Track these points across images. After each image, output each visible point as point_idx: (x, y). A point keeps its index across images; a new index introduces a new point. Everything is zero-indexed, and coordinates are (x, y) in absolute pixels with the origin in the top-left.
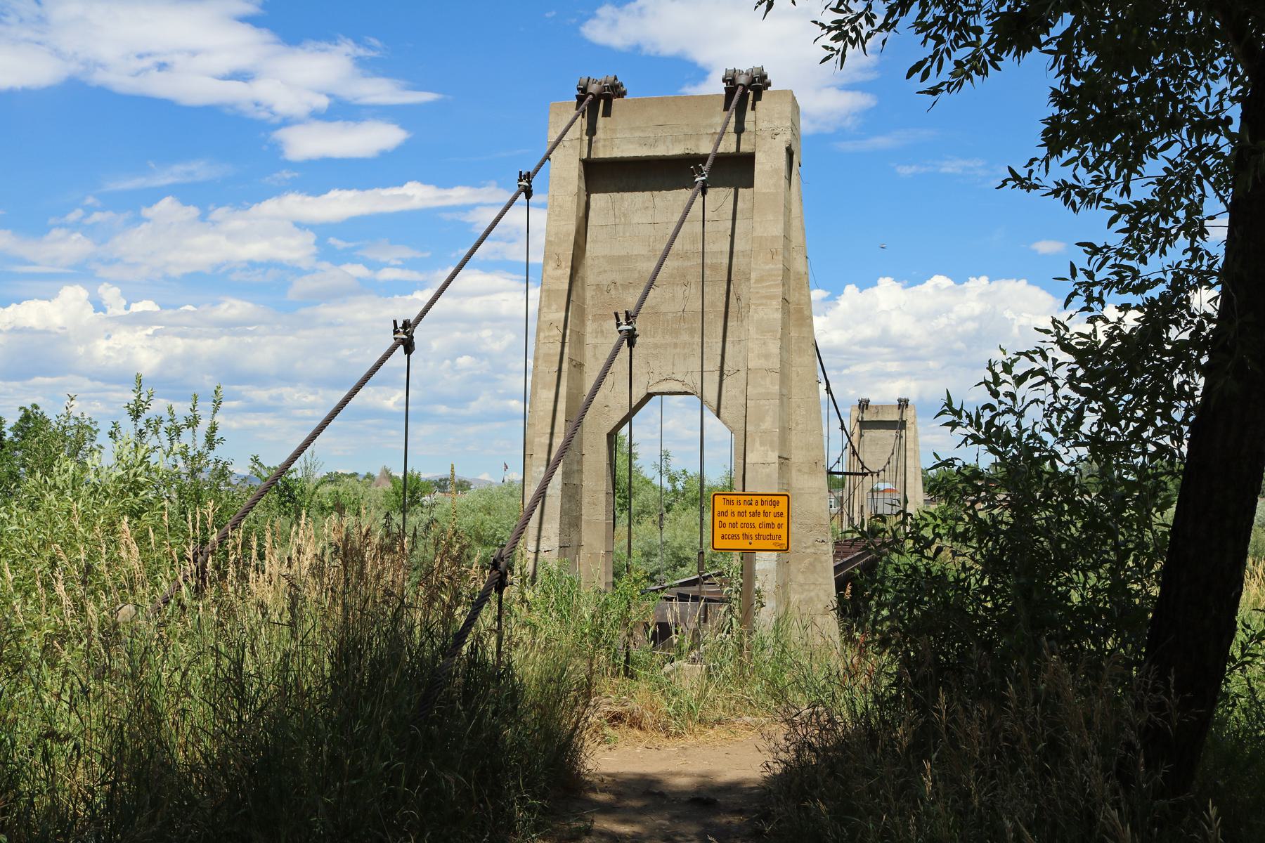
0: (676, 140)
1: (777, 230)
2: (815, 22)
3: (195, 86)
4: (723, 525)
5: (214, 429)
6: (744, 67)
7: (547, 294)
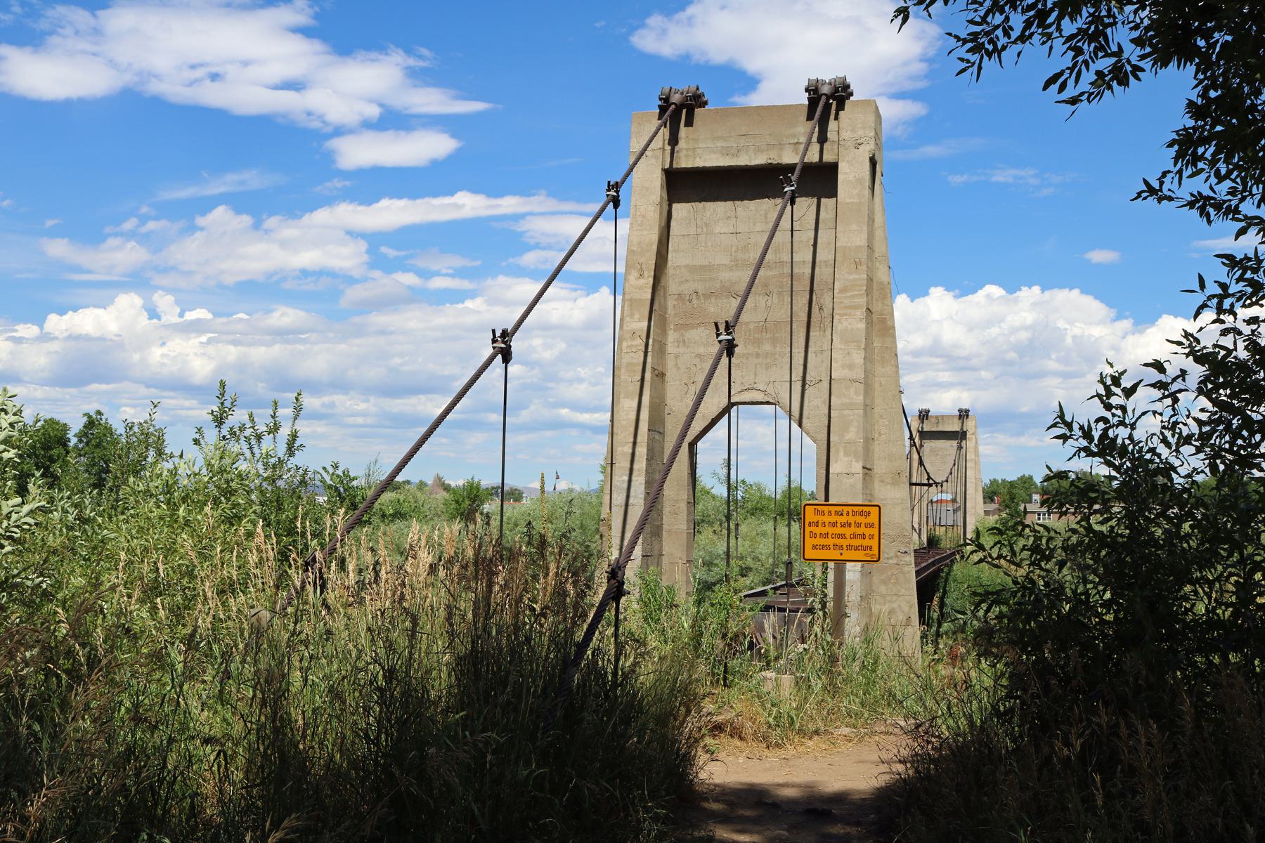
0: (759, 150)
1: (860, 240)
2: (950, 34)
3: (247, 95)
4: (813, 535)
5: (294, 436)
6: (827, 77)
7: (631, 303)
